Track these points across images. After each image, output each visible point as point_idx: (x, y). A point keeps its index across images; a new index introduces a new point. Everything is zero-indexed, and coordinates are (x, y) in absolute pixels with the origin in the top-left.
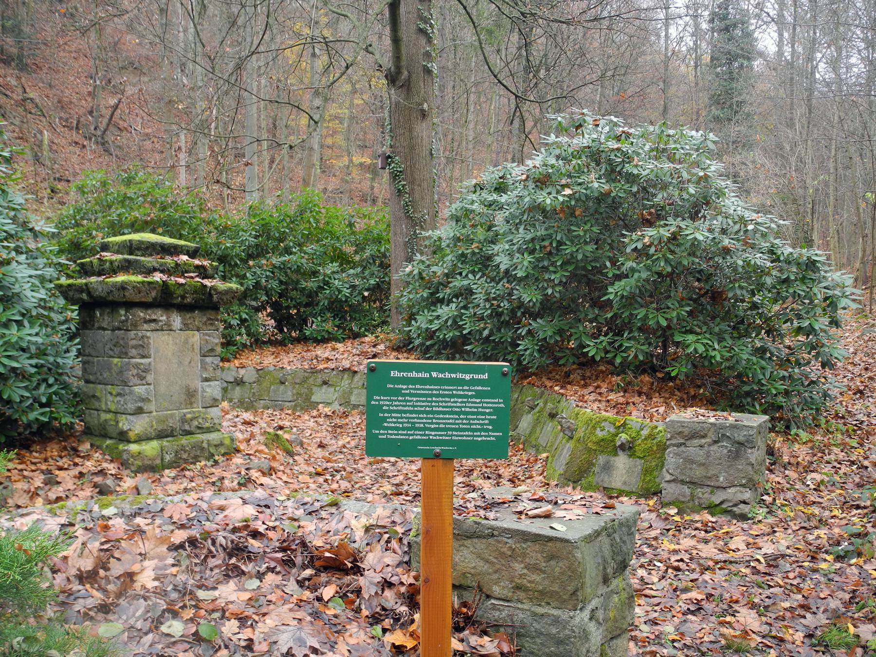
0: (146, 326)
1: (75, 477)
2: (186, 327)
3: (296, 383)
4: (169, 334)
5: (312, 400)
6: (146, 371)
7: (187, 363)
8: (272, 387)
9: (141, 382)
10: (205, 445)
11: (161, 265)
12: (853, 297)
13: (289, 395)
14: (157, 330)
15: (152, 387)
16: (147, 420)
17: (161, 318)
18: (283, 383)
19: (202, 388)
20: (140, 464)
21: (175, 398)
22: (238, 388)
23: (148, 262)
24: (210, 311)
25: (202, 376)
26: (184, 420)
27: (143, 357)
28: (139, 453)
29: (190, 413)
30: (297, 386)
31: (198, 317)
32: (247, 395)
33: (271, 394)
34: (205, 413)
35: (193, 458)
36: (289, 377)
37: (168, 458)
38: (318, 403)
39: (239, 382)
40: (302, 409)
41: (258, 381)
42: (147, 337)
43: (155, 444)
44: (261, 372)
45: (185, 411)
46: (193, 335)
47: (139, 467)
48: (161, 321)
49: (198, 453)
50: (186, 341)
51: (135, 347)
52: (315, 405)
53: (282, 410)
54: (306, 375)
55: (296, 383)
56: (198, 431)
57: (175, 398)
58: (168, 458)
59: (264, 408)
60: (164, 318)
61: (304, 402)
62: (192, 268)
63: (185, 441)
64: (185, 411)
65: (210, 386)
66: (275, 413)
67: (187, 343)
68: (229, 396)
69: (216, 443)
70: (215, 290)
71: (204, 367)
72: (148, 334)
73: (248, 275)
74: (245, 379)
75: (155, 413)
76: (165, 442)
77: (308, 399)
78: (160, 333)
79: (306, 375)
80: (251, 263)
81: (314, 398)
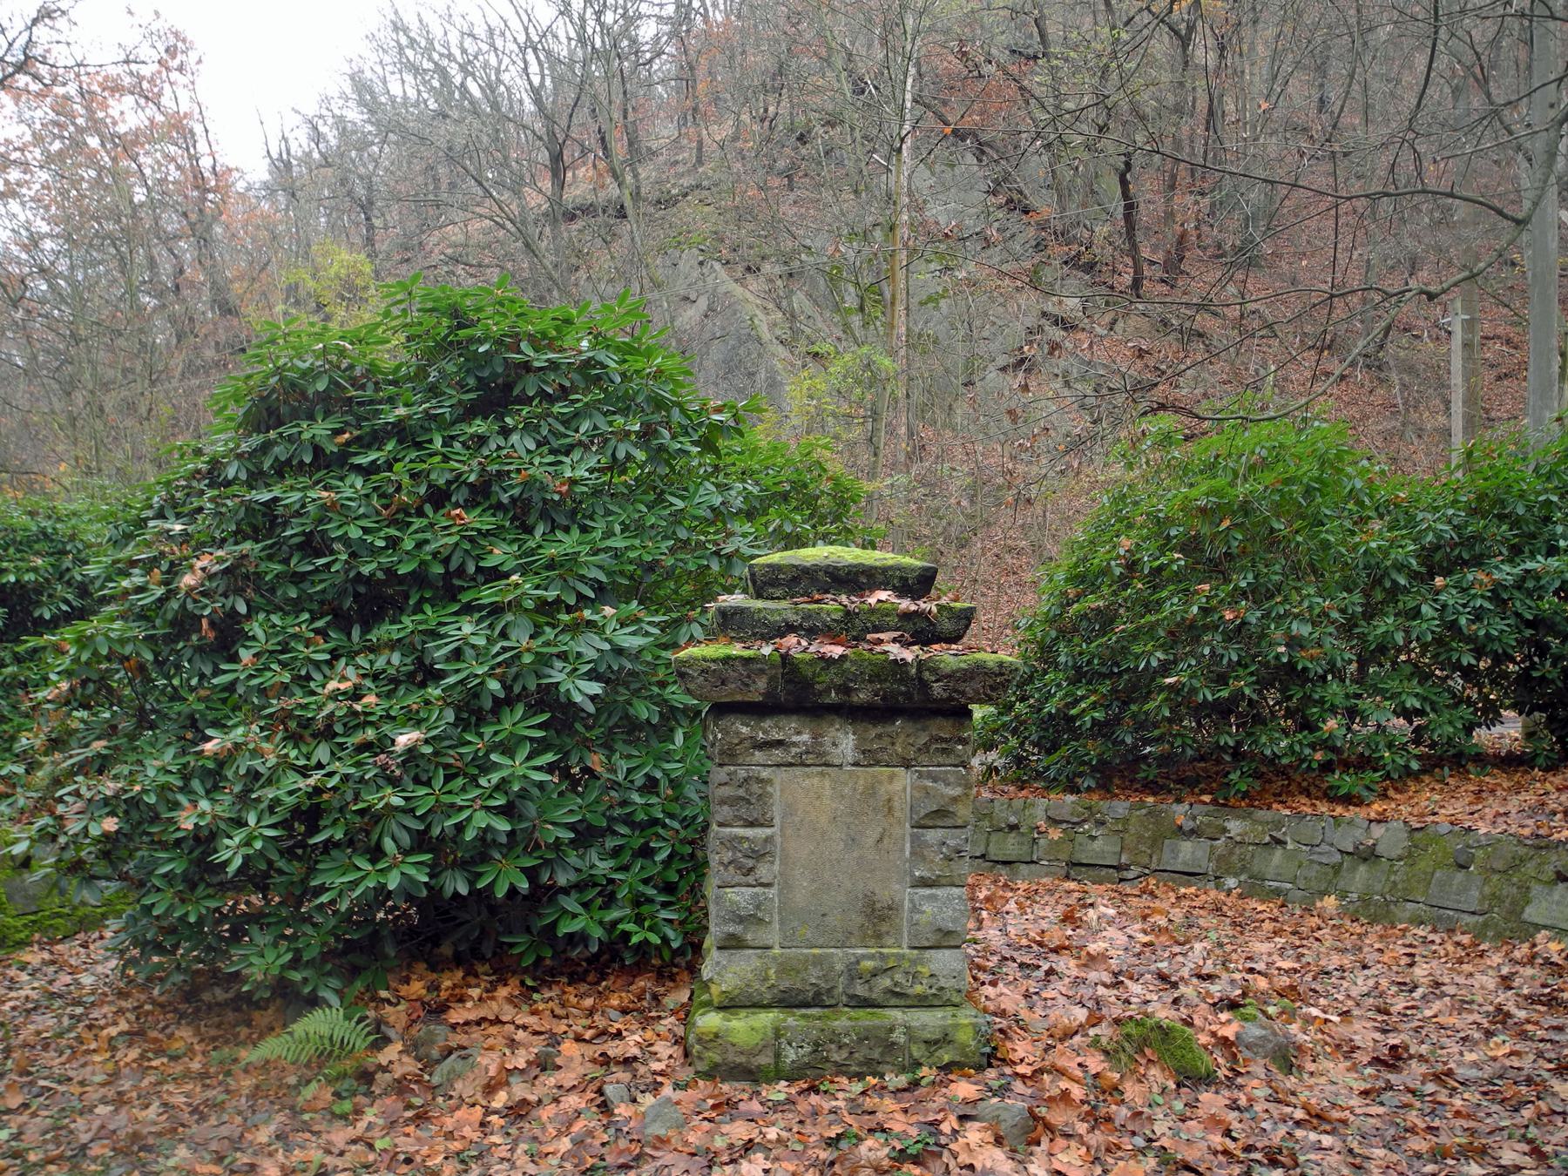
0: (759, 756)
1: (594, 1061)
2: (869, 757)
3: (1494, 871)
4: (822, 774)
5: (1525, 916)
6: (758, 856)
7: (871, 841)
8: (1438, 874)
9: (744, 879)
10: (899, 1037)
11: (807, 616)
13: (1473, 898)
14: (791, 765)
15: (772, 892)
17: (795, 739)
18: (1463, 867)
19: (912, 901)
20: (718, 1059)
21: (834, 920)
22: (1362, 868)
23: (772, 611)
24: (940, 721)
25: (912, 875)
26: (853, 973)
27: (751, 824)
28: (717, 1036)
29: (872, 957)
30: (1495, 877)
31: (903, 735)
32: (1378, 887)
33: (1433, 889)
35: (860, 1064)
36: (1480, 853)
37: (791, 1055)
38: (1538, 927)
39: (1368, 855)
40: (1498, 936)
41: (1409, 857)
42: (760, 781)
43: (766, 1019)
44: (1418, 835)
45: (860, 951)
46: (891, 778)
47: (716, 1066)
48: (795, 744)
49: (876, 1055)
50: (871, 791)
51: (732, 801)
52: (1528, 931)
53: (1451, 931)
54: (1522, 851)
55: (1494, 871)
56: (893, 1001)
57: (834, 920)
58: (791, 1055)
59: (1411, 922)
60: (805, 737)
61: (1507, 920)
63: (844, 1021)
64: (860, 951)
65: (933, 898)
66: (1431, 937)
68: (1341, 885)
70: (934, 671)
71: (918, 853)
72: (765, 773)
73: (1425, 609)
74: (1380, 850)
75: (777, 951)
76: (792, 1020)
77: (1515, 911)
78: (798, 771)
79: (1522, 851)
80: (1439, 581)
81: (1531, 913)
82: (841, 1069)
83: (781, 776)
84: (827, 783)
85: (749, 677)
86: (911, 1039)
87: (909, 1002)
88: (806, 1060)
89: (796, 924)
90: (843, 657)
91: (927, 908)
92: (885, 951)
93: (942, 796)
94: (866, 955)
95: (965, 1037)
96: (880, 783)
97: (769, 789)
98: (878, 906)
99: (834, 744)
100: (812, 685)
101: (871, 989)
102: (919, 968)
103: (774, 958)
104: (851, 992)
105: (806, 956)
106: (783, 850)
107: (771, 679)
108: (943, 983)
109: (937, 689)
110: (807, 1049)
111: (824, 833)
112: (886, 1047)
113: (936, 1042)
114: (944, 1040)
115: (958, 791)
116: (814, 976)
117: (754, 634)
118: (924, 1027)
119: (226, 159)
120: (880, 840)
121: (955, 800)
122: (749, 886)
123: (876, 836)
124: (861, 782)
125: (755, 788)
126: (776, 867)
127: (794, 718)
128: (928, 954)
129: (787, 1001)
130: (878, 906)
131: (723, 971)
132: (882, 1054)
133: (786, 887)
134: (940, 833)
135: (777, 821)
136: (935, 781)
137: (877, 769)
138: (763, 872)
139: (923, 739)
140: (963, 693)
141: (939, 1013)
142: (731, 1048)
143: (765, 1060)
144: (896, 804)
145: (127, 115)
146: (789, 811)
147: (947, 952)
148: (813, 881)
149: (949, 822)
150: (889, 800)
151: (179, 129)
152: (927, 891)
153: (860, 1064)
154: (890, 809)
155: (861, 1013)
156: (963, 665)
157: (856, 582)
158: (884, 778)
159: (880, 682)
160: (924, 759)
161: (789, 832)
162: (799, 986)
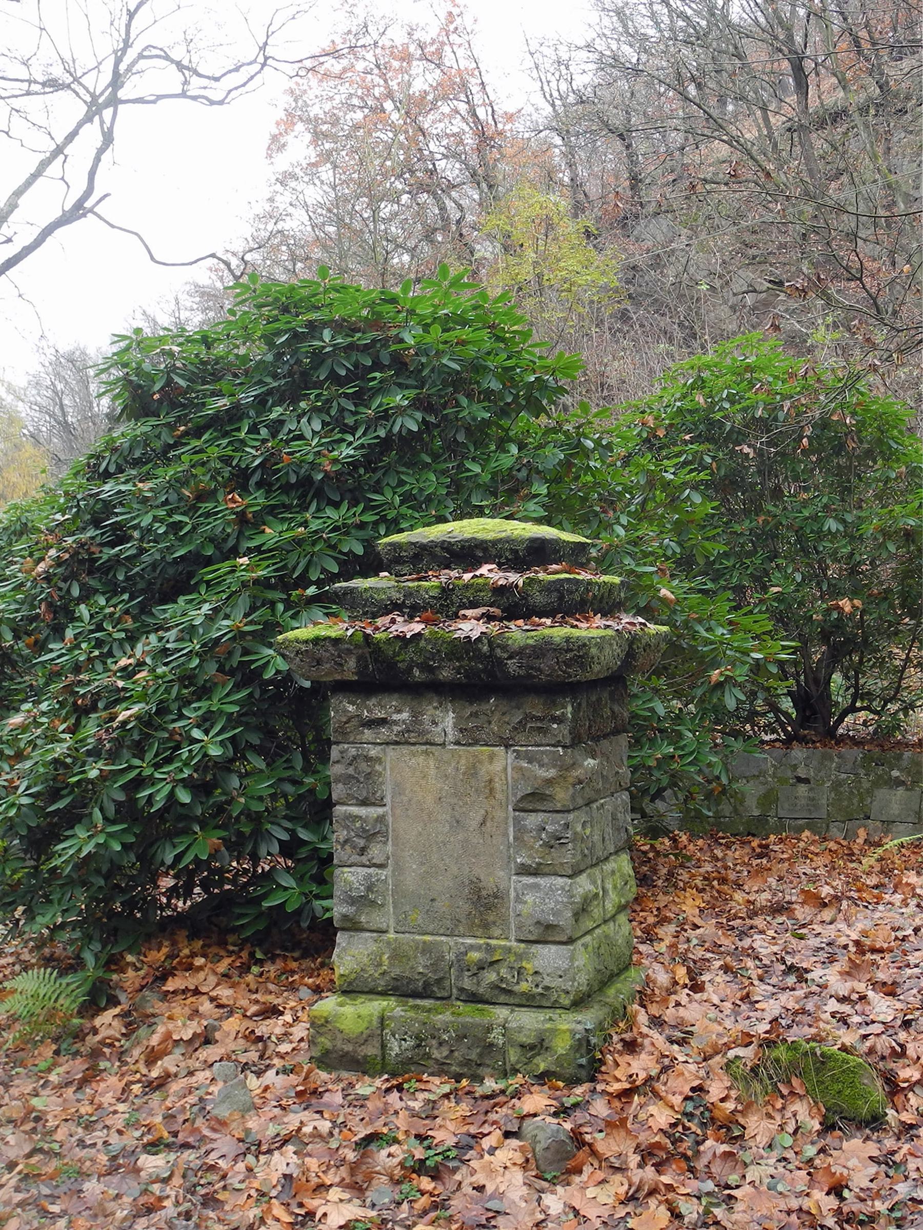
0: (368, 734)
2: (469, 737)
4: (426, 753)
6: (370, 837)
7: (474, 824)
10: (496, 1037)
11: (409, 594)
12: (651, 558)
14: (397, 743)
16: (373, 947)
17: (395, 717)
20: (329, 1045)
21: (442, 905)
27: (364, 803)
29: (478, 948)
31: (497, 714)
34: (520, 957)
35: (461, 1064)
42: (368, 759)
43: (374, 1007)
45: (469, 941)
46: (491, 757)
48: (395, 723)
49: (473, 1055)
50: (472, 771)
51: (347, 779)
56: (502, 998)
58: (395, 1047)
62: (487, 596)
65: (536, 886)
67: (475, 775)
69: (524, 1039)
70: (504, 648)
72: (374, 752)
75: (392, 935)
78: (405, 749)
82: (441, 1070)
83: (391, 753)
84: (432, 763)
85: (339, 656)
86: (510, 1042)
87: (517, 1001)
88: (409, 1054)
89: (407, 908)
90: (419, 635)
91: (529, 898)
92: (493, 942)
93: (536, 778)
94: (473, 947)
95: (562, 1045)
96: (480, 762)
97: (378, 768)
98: (484, 893)
99: (435, 723)
100: (396, 663)
101: (478, 983)
102: (524, 964)
103: (389, 943)
104: (460, 984)
105: (417, 943)
106: (393, 830)
107: (360, 659)
108: (547, 981)
109: (512, 665)
110: (411, 1043)
111: (430, 814)
112: (485, 1047)
113: (532, 1047)
114: (539, 1046)
115: (552, 773)
116: (421, 965)
117: (365, 613)
118: (520, 1029)
119: (505, 106)
120: (483, 823)
121: (549, 782)
122: (364, 866)
123: (479, 818)
124: (463, 762)
125: (364, 766)
126: (389, 848)
127: (396, 696)
128: (534, 948)
129: (401, 989)
130: (484, 893)
131: (350, 955)
132: (481, 1055)
133: (399, 869)
134: (541, 817)
135: (388, 800)
136: (530, 762)
137: (478, 748)
138: (376, 852)
139: (518, 717)
140: (539, 669)
141: (542, 1015)
142: (339, 1036)
143: (372, 1050)
144: (497, 785)
145: (423, 79)
146: (399, 789)
147: (553, 948)
148: (422, 864)
149: (549, 806)
150: (491, 781)
151: (456, 87)
152: (531, 880)
153: (461, 1064)
154: (492, 790)
155: (470, 1007)
156: (531, 642)
157: (474, 556)
158: (484, 758)
159: (458, 660)
160: (521, 738)
161: (398, 812)
162: (407, 974)
